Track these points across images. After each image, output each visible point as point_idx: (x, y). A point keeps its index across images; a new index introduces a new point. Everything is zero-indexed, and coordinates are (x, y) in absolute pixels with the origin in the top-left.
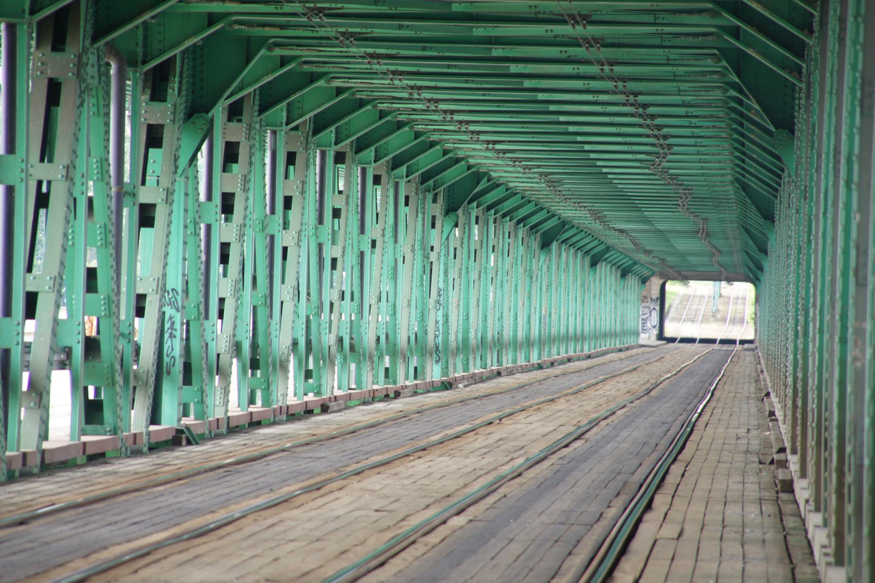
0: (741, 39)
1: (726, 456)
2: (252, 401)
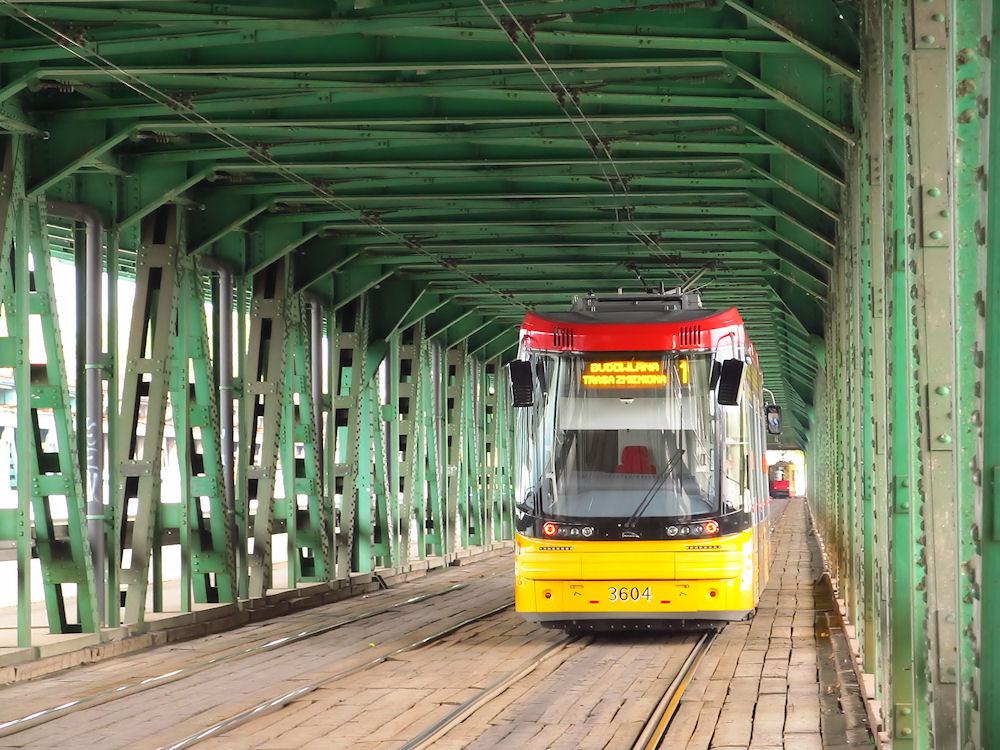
0: (754, 5)
2: (378, 564)
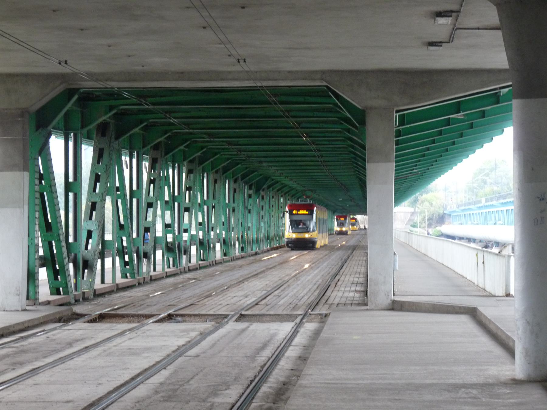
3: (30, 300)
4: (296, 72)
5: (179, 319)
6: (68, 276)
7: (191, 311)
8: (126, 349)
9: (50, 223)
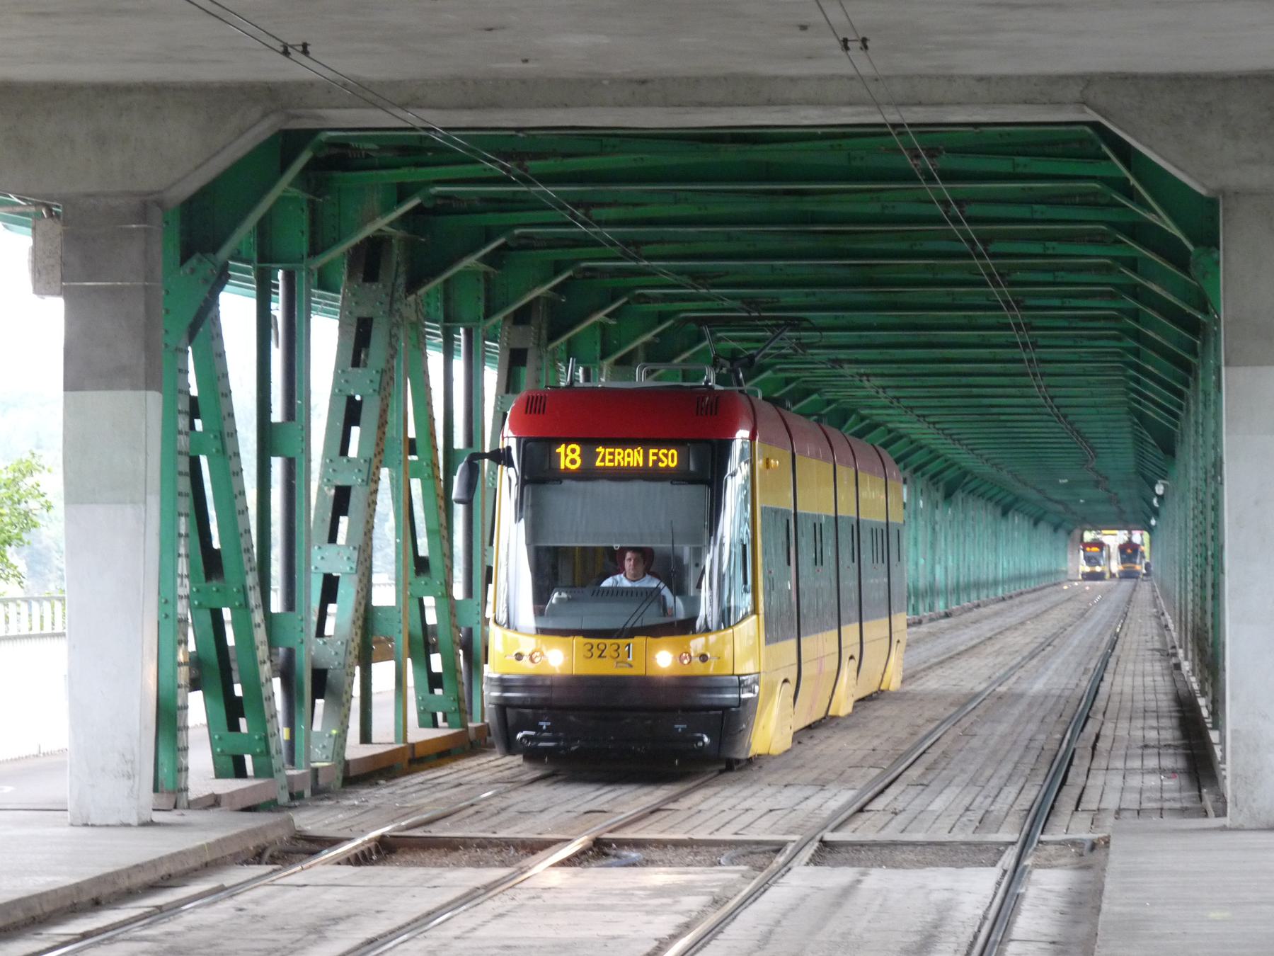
1: (1141, 653)
3: (163, 792)
4: (1004, 79)
5: (634, 855)
6: (272, 717)
7: (662, 832)
8: (497, 947)
9: (218, 551)
